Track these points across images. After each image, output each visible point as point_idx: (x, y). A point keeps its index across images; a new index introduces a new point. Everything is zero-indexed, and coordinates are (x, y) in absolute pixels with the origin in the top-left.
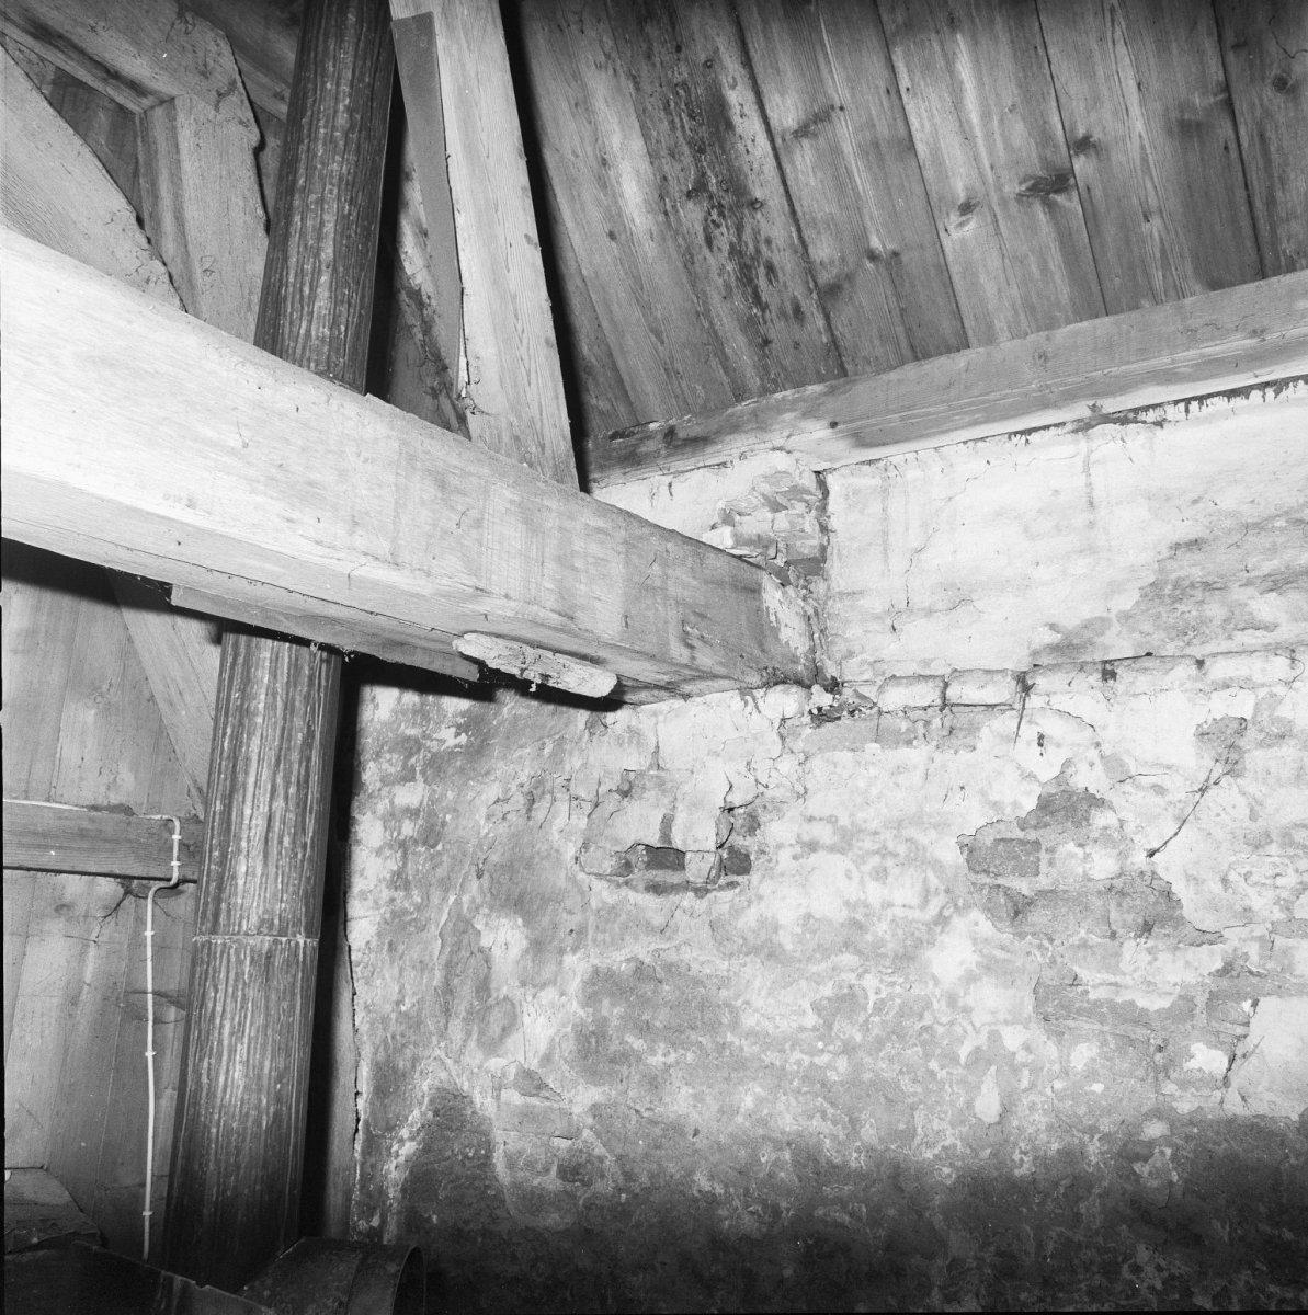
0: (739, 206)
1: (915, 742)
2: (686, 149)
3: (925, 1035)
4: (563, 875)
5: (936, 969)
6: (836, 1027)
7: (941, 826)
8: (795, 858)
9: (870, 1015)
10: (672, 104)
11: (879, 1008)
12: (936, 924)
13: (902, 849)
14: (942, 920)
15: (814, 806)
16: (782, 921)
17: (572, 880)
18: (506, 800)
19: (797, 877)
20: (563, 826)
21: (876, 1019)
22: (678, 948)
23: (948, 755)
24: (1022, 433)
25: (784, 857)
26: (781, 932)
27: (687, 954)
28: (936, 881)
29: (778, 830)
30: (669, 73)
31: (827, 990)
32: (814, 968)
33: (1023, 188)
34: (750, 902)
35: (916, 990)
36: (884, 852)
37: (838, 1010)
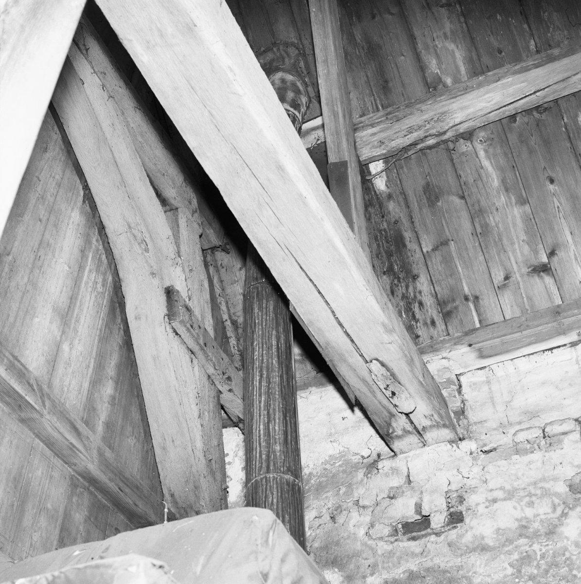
0: (407, 277)
1: (535, 452)
2: (384, 254)
3: (568, 562)
4: (359, 543)
5: (566, 534)
6: (523, 571)
7: (555, 479)
8: (487, 507)
9: (539, 561)
10: (379, 238)
11: (543, 557)
12: (562, 517)
13: (539, 492)
14: (564, 515)
15: (491, 485)
16: (485, 535)
17: (365, 544)
18: (320, 517)
19: (490, 515)
20: (356, 523)
21: (542, 562)
22: (432, 559)
23: (552, 453)
24: (549, 350)
25: (481, 509)
26: (486, 539)
27: (437, 561)
28: (558, 501)
29: (472, 499)
30: (378, 226)
31: (516, 556)
32: (506, 549)
33: (530, 270)
34: (467, 531)
35: (559, 545)
36: (530, 495)
37: (522, 564)
